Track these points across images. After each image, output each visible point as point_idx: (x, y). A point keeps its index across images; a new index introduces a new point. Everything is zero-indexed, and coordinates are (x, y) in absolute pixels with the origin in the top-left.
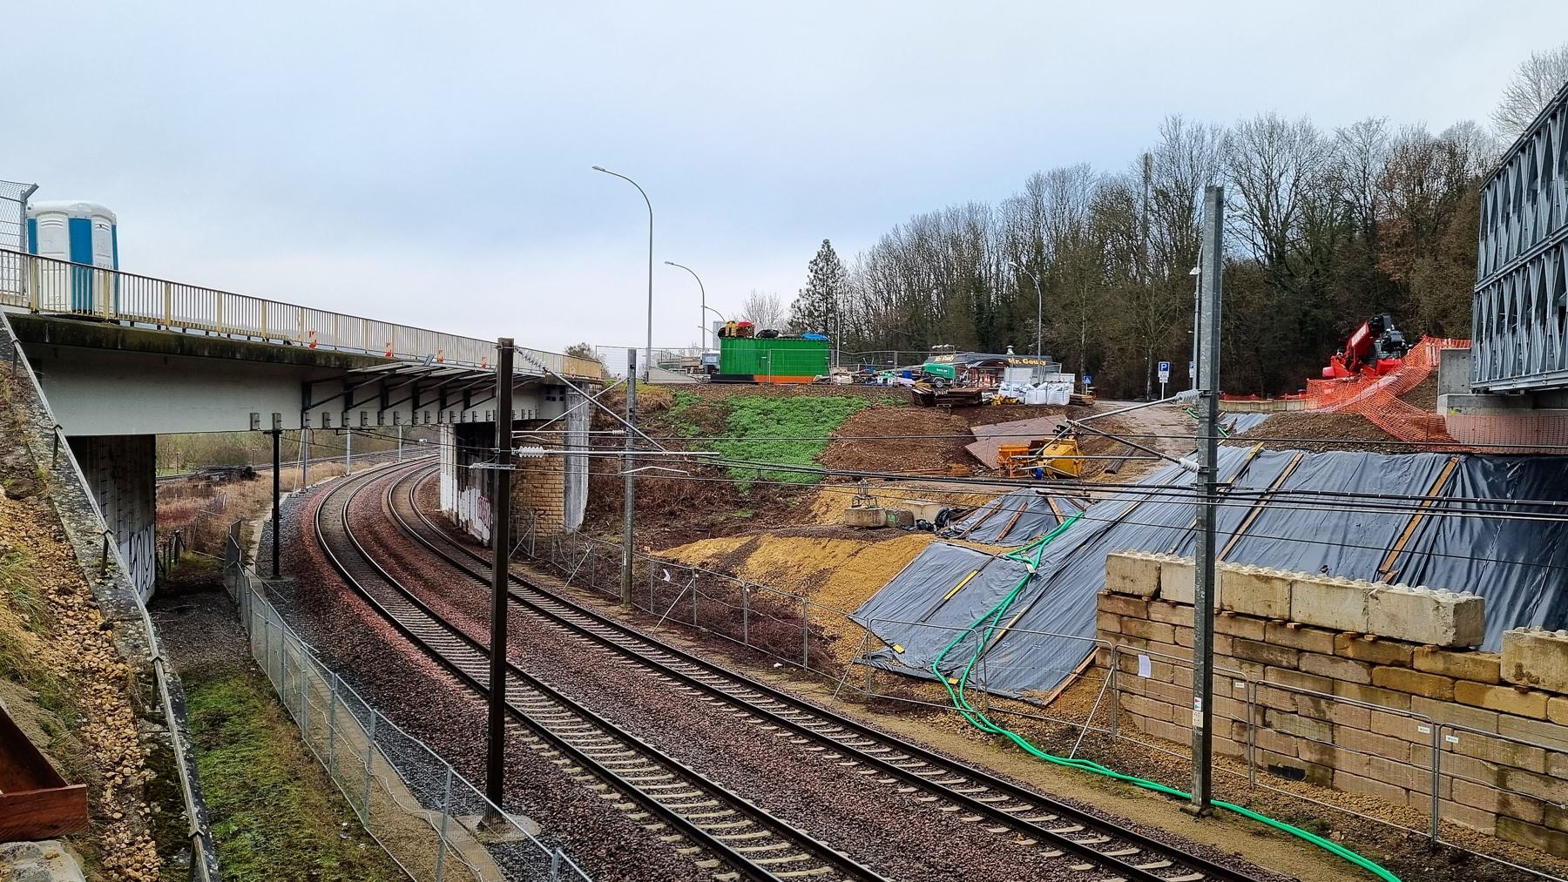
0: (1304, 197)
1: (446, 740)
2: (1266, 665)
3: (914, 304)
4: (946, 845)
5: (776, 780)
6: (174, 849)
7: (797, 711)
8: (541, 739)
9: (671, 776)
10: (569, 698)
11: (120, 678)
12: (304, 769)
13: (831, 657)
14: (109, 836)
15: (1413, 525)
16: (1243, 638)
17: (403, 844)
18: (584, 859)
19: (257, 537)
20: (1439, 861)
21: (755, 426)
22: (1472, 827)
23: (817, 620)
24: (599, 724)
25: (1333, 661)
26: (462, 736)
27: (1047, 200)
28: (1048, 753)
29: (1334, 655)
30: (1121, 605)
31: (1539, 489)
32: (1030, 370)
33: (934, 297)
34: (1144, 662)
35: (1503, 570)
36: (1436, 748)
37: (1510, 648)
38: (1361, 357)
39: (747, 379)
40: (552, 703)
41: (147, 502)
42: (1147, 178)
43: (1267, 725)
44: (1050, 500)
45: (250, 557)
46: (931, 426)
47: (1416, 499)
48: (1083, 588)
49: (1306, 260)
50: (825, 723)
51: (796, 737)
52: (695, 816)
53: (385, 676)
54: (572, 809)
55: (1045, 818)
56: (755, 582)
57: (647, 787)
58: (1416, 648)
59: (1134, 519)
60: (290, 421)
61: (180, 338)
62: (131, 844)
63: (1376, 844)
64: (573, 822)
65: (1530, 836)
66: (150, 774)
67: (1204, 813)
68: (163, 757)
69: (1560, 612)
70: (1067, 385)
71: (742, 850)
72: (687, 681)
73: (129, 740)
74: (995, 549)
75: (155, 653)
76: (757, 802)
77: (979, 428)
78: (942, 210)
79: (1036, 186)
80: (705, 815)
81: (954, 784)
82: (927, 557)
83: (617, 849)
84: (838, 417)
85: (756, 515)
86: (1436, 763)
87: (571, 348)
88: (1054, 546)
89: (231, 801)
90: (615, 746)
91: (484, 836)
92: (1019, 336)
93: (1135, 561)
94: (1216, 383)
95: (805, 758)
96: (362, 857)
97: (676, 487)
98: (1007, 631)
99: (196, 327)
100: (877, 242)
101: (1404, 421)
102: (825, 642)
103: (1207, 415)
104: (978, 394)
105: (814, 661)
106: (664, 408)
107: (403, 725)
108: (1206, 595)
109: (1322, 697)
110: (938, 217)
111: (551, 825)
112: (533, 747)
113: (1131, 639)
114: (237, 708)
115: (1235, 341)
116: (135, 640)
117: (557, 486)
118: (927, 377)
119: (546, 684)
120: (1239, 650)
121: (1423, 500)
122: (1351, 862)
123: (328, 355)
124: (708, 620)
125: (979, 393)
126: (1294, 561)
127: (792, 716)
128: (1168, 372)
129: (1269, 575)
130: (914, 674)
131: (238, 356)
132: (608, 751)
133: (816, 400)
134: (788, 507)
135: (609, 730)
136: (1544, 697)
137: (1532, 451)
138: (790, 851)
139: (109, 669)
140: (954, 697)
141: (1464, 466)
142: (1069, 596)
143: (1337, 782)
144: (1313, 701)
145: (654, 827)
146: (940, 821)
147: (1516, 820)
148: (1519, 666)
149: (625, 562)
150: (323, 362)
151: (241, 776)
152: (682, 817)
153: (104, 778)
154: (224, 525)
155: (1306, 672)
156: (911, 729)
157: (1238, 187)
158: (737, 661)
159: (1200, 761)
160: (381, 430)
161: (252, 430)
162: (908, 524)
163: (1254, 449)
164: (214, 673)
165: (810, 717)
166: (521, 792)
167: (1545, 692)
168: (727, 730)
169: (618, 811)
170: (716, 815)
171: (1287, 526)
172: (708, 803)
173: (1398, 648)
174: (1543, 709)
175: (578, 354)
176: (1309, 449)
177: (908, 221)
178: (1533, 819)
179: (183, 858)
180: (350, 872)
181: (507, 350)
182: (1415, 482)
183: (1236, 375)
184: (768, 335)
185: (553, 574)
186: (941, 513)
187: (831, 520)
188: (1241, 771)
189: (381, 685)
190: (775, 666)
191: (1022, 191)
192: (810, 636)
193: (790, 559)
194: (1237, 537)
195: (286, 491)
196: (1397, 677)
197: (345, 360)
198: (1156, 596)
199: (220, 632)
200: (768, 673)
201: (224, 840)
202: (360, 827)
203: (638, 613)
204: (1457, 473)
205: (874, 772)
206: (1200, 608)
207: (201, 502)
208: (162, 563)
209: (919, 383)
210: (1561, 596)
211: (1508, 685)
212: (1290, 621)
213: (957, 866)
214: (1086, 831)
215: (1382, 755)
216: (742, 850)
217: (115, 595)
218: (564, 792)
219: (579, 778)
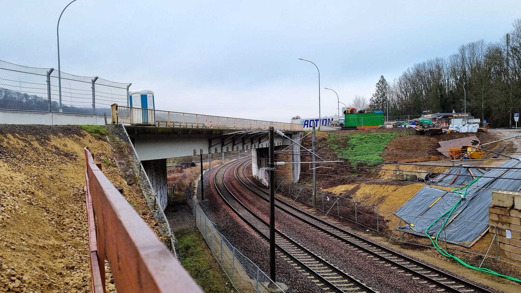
3: (416, 96)
7: (375, 248)
10: (296, 242)
12: (214, 265)
13: (387, 228)
21: (357, 144)
23: (382, 215)
27: (467, 55)
28: (471, 265)
30: (499, 211)
33: (424, 93)
39: (354, 128)
40: (291, 243)
42: (508, 43)
44: (470, 170)
46: (423, 142)
50: (385, 252)
53: (237, 234)
54: (298, 281)
57: (323, 274)
64: (299, 286)
74: (448, 189)
77: (442, 142)
78: (426, 61)
79: (463, 50)
81: (434, 277)
82: (422, 192)
84: (388, 140)
93: (503, 194)
95: (378, 265)
104: (441, 130)
110: (424, 64)
113: (503, 223)
116: (164, 229)
117: (290, 167)
118: (421, 124)
119: (288, 237)
124: (343, 214)
127: (373, 250)
130: (418, 234)
131: (190, 133)
132: (310, 261)
133: (379, 134)
134: (370, 173)
140: (434, 244)
151: (195, 267)
154: (187, 182)
158: (353, 229)
162: (414, 179)
164: (186, 232)
169: (313, 283)
170: (347, 285)
172: (344, 281)
177: (413, 66)
185: (290, 197)
186: (427, 175)
187: (386, 178)
191: (457, 52)
192: (379, 220)
193: (371, 192)
198: (513, 207)
199: (187, 219)
200: (365, 233)
202: (231, 285)
209: (418, 126)
217: (158, 215)
219: (300, 271)
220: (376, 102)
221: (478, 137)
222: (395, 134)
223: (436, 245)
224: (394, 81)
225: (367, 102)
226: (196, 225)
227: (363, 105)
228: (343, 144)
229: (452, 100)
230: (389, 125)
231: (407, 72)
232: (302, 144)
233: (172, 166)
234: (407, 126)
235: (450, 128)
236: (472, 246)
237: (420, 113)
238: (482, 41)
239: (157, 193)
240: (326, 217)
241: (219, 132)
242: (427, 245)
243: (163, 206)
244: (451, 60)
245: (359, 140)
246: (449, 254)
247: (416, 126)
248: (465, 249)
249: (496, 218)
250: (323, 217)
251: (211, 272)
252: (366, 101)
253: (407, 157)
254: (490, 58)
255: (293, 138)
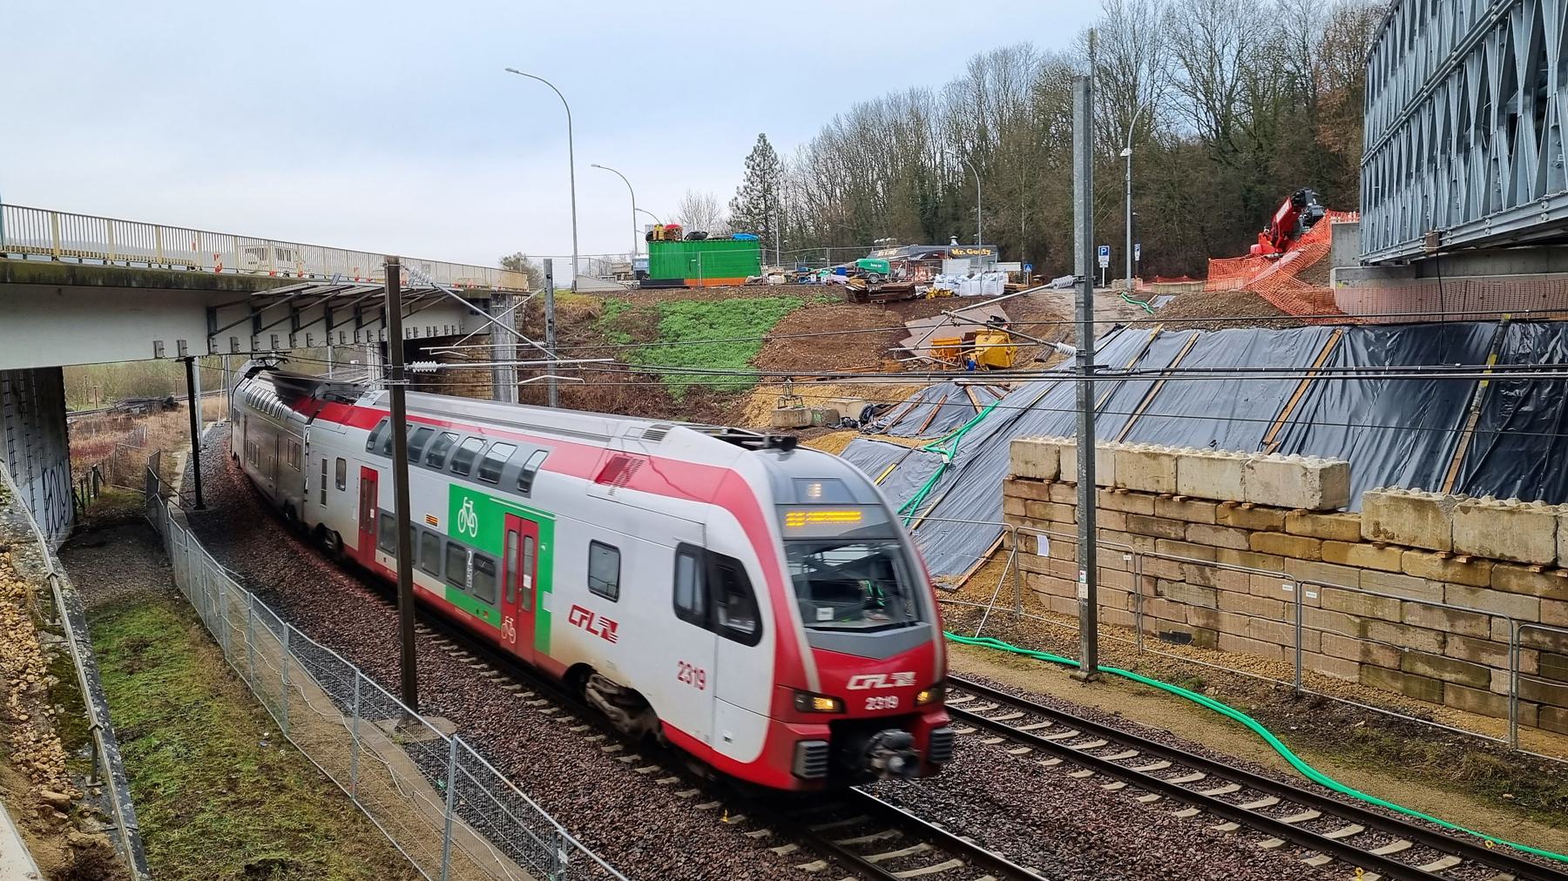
0: (1247, 68)
2: (1157, 538)
3: (858, 195)
6: (80, 743)
11: (20, 596)
14: (16, 736)
16: (1136, 514)
20: (1300, 707)
21: (687, 331)
22: (1339, 676)
25: (1216, 530)
28: (955, 633)
29: (1216, 524)
30: (1025, 488)
31: (1415, 356)
32: (968, 261)
33: (879, 189)
34: (1042, 540)
35: (1376, 436)
36: (1299, 604)
37: (1369, 507)
39: (677, 283)
41: (59, 437)
42: (1092, 54)
43: (1158, 594)
44: (969, 390)
45: (173, 489)
46: (866, 323)
49: (1250, 134)
53: (310, 597)
58: (1288, 513)
59: (1042, 405)
60: (196, 348)
61: (71, 269)
62: (38, 742)
65: (1389, 680)
66: (53, 680)
67: (1091, 678)
69: (1425, 472)
70: (1001, 274)
73: (32, 650)
74: (911, 443)
78: (883, 97)
79: (978, 68)
84: (771, 318)
86: (1299, 618)
87: (506, 259)
89: (154, 719)
91: (401, 737)
92: (965, 227)
93: (1036, 445)
94: (1090, 270)
96: (281, 761)
97: (609, 397)
98: (923, 520)
99: (92, 255)
100: (818, 134)
106: (593, 317)
108: (1087, 473)
109: (1207, 565)
110: (879, 105)
112: (453, 654)
113: (1035, 521)
114: (160, 634)
116: (33, 560)
118: (862, 274)
121: (1308, 371)
122: (1220, 713)
123: (229, 279)
125: (912, 287)
126: (1186, 438)
129: (1158, 452)
131: (134, 284)
133: (748, 302)
136: (1398, 551)
139: (9, 588)
141: (1347, 337)
142: (981, 482)
147: (1377, 667)
148: (1377, 524)
151: (164, 695)
153: (10, 685)
154: (142, 458)
157: (1181, 62)
159: (1087, 630)
160: (311, 352)
161: (156, 358)
163: (1155, 331)
166: (439, 697)
171: (1182, 404)
175: (514, 265)
176: (1206, 328)
177: (849, 110)
178: (1392, 665)
179: (87, 751)
181: (393, 268)
182: (1301, 354)
183: (1182, 256)
184: (697, 237)
186: (865, 410)
188: (1132, 638)
189: (305, 606)
191: (964, 74)
196: (1272, 542)
197: (248, 283)
198: (1056, 478)
199: (142, 563)
201: (148, 754)
202: (281, 736)
204: (1340, 345)
207: (121, 435)
208: (80, 498)
211: (1368, 542)
217: (11, 520)
220: (745, 211)
221: (1004, 308)
222: (790, 302)
227: (710, 220)
228: (646, 332)
229: (950, 210)
230: (775, 276)
233: (94, 412)
234: (824, 279)
235: (935, 285)
236: (962, 586)
237: (868, 246)
238: (1028, 47)
239: (31, 485)
241: (240, 286)
245: (690, 319)
247: (847, 279)
249: (1019, 510)
252: (717, 209)
254: (1045, 93)
255: (492, 311)
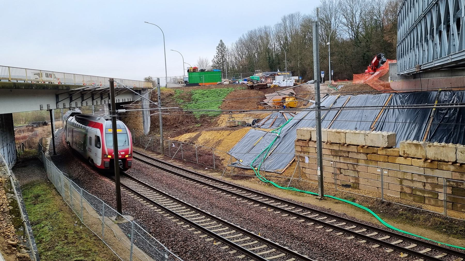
1: (106, 197)
2: (340, 157)
3: (250, 57)
4: (249, 213)
5: (203, 200)
6: (19, 226)
7: (210, 181)
8: (132, 192)
9: (172, 201)
10: (143, 182)
12: (64, 208)
13: (222, 165)
15: (380, 114)
17: (93, 226)
18: (146, 225)
19: (49, 143)
21: (200, 99)
23: (217, 155)
24: (152, 189)
26: (111, 195)
27: (288, 23)
28: (282, 186)
29: (357, 152)
30: (301, 143)
31: (414, 102)
33: (256, 56)
34: (306, 158)
35: (403, 125)
37: (402, 146)
38: (376, 66)
39: (197, 84)
40: (139, 184)
41: (12, 134)
42: (318, 15)
43: (341, 173)
44: (284, 114)
45: (47, 149)
47: (381, 107)
48: (292, 139)
50: (218, 183)
51: (209, 187)
52: (178, 211)
53: (88, 180)
54: (142, 212)
55: (278, 204)
56: (200, 145)
57: (165, 205)
58: (378, 149)
59: (305, 118)
60: (53, 106)
61: (14, 84)
62: (7, 226)
63: (368, 203)
64: (143, 216)
65: (409, 197)
66: (11, 208)
67: (322, 199)
68: (14, 202)
71: (191, 219)
72: (178, 175)
73: (4, 199)
74: (267, 130)
75: (10, 174)
76: (197, 206)
77: (267, 95)
78: (257, 29)
79: (284, 20)
80: (181, 211)
81: (254, 197)
82: (249, 134)
83: (155, 222)
84: (225, 94)
85: (202, 125)
86: (382, 179)
87: (146, 78)
88: (284, 128)
89: (42, 218)
90: (156, 195)
91: (117, 222)
92: (282, 66)
93: (304, 130)
95: (211, 193)
98: (271, 153)
99: (21, 80)
100: (237, 39)
101: (379, 85)
102: (220, 161)
103: (317, 87)
104: (266, 85)
105: (217, 167)
107: (94, 194)
108: (319, 138)
109: (355, 164)
110: (255, 31)
111: (136, 218)
113: (304, 152)
114: (43, 193)
115: (345, 63)
116: (4, 172)
117: (141, 121)
118: (252, 81)
119: (137, 179)
120: (333, 153)
121: (383, 107)
122: (360, 208)
124: (187, 157)
125: (267, 84)
126: (348, 127)
127: (209, 182)
128: (324, 74)
129: (340, 131)
130: (245, 167)
131: (34, 88)
132: (154, 196)
133: (218, 90)
134: (211, 122)
135: (155, 190)
136: (410, 159)
137: (414, 91)
138: (205, 218)
140: (256, 173)
142: (287, 142)
143: (360, 188)
144: (353, 166)
145: (166, 215)
146: (247, 207)
147: (405, 193)
148: (404, 151)
149: (161, 142)
150: (61, 88)
151: (45, 211)
152: (174, 212)
154: (37, 140)
155: (350, 158)
156: (244, 183)
157: (344, 17)
158: (195, 168)
160: (88, 107)
161: (41, 110)
162: (245, 124)
163: (338, 96)
164: (36, 183)
165: (214, 182)
167: (411, 157)
168: (189, 187)
169: (156, 212)
170: (184, 210)
172: (183, 208)
173: (374, 149)
174: (411, 162)
175: (148, 80)
176: (353, 95)
177: (247, 32)
178: (410, 192)
179: (22, 229)
180: (77, 234)
181: (112, 82)
184: (202, 71)
185: (141, 147)
186: (254, 121)
187: (223, 125)
188: (334, 187)
190: (206, 169)
191: (280, 21)
192: (216, 159)
193: (210, 137)
194: (333, 121)
195: (58, 128)
196: (374, 157)
197: (68, 87)
198: (310, 140)
199: (37, 171)
200: (204, 171)
201: (40, 229)
202: (81, 222)
203: (166, 157)
204: (392, 99)
205: (230, 195)
206: (318, 142)
207: (30, 133)
208: (18, 152)
209: (249, 82)
210: (418, 131)
212: (345, 144)
213: (251, 218)
214: (288, 206)
215: (371, 179)
216: (191, 219)
218: (140, 208)
219: (145, 204)
220: (217, 63)
221: (294, 90)
223: (258, 174)
224: (232, 45)
225: (209, 63)
226: (47, 177)
227: (206, 65)
228: (188, 99)
229: (277, 61)
230: (226, 82)
231: (242, 37)
232: (151, 99)
233: (22, 126)
234: (240, 82)
237: (253, 72)
240: (173, 161)
242: (251, 175)
243: (12, 162)
244: (276, 29)
245: (201, 95)
246: (267, 180)
248: (278, 175)
250: (169, 161)
251: (61, 214)
252: (208, 62)
253: (240, 108)
